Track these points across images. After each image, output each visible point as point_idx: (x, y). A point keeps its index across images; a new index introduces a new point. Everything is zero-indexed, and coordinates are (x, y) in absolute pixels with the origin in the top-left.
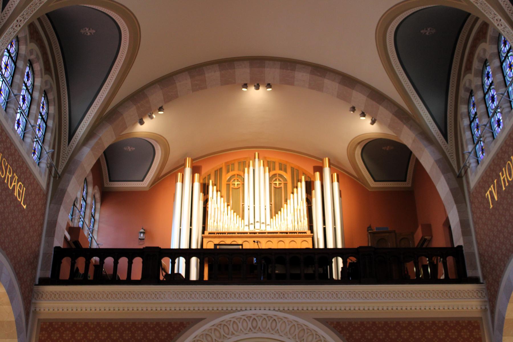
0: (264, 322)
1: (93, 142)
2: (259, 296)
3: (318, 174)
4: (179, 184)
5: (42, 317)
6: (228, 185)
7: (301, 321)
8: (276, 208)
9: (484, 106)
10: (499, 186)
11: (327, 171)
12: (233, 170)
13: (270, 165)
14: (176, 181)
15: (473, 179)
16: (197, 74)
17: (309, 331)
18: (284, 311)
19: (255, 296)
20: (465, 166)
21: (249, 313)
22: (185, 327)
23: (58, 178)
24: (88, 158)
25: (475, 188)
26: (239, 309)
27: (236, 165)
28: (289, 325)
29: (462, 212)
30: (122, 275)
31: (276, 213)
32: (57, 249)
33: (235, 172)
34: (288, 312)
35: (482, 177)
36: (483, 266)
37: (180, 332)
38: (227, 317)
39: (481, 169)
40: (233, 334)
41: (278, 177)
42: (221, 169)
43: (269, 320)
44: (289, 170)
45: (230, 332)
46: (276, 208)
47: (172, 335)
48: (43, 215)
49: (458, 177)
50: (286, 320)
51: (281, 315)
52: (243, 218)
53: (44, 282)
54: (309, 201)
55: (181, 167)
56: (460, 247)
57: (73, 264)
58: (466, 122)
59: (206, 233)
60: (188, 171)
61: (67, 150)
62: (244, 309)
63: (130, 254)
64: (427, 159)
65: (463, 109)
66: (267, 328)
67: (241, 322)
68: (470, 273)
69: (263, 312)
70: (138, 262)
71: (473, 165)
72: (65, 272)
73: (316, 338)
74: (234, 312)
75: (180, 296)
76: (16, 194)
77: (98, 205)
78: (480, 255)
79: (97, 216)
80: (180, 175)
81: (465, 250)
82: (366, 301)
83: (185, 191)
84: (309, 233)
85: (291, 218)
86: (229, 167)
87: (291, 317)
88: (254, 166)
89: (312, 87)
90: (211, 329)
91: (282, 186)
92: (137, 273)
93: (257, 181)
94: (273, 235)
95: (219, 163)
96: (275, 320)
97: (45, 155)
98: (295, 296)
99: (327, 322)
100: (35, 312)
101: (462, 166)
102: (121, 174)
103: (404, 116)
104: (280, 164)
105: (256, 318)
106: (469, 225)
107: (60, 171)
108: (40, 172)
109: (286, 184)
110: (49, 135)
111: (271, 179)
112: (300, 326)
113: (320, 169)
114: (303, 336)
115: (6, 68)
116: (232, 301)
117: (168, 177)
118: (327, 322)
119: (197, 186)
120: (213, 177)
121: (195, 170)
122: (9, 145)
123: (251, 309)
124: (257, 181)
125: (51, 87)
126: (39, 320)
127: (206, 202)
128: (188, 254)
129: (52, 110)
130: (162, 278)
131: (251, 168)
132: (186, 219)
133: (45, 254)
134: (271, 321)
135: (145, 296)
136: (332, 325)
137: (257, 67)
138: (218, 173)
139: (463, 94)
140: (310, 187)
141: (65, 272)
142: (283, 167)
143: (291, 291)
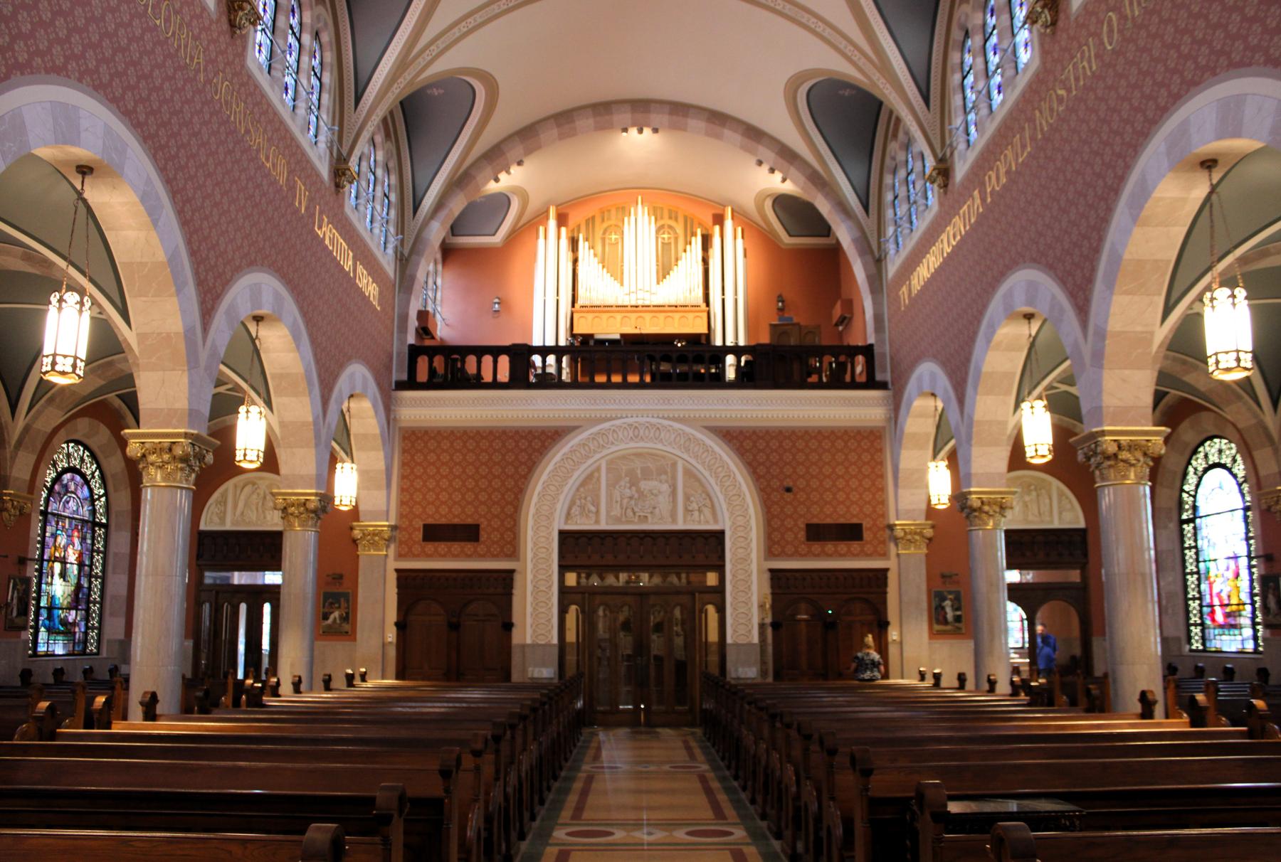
1: (443, 214)
3: (717, 228)
4: (541, 240)
5: (403, 425)
6: (603, 240)
7: (688, 430)
8: (664, 271)
9: (1007, 16)
10: (910, 290)
11: (729, 223)
12: (609, 219)
13: (656, 212)
14: (537, 237)
15: (892, 268)
16: (564, 121)
18: (668, 418)
20: (951, 145)
21: (630, 420)
23: (405, 262)
24: (436, 232)
25: (962, 183)
27: (613, 212)
29: (877, 304)
30: (487, 377)
31: (664, 277)
32: (411, 346)
33: (612, 222)
34: (674, 419)
35: (1023, 94)
36: (892, 372)
38: (607, 425)
39: (972, 156)
41: (666, 229)
42: (593, 218)
44: (681, 219)
46: (664, 271)
48: (393, 309)
49: (877, 262)
51: (666, 423)
52: (622, 285)
53: (401, 386)
54: (705, 261)
55: (542, 217)
56: (871, 346)
57: (431, 362)
58: (957, 77)
59: (577, 306)
60: (552, 223)
61: (413, 225)
63: (496, 351)
64: (844, 234)
65: (955, 57)
68: (879, 377)
70: (504, 361)
71: (962, 146)
72: (422, 376)
76: (327, 242)
77: (440, 267)
78: (892, 359)
79: (439, 282)
80: (541, 229)
81: (877, 350)
83: (549, 247)
84: (703, 306)
85: (683, 284)
86: (604, 213)
87: (677, 425)
88: (636, 214)
89: (708, 134)
91: (672, 241)
92: (504, 375)
93: (640, 233)
94: (659, 308)
95: (590, 210)
97: (324, 128)
100: (395, 419)
101: (948, 142)
102: (475, 247)
103: (818, 180)
104: (670, 211)
106: (883, 321)
107: (406, 252)
108: (320, 158)
109: (676, 239)
110: (325, 97)
111: (657, 232)
113: (719, 220)
115: (265, 10)
117: (528, 228)
119: (564, 242)
120: (583, 228)
121: (562, 220)
122: (198, 11)
124: (640, 233)
125: (326, 24)
126: (400, 428)
127: (575, 261)
128: (558, 351)
129: (329, 57)
130: (532, 379)
131: (633, 218)
132: (553, 293)
133: (398, 354)
137: (642, 110)
138: (590, 221)
139: (957, 35)
140: (706, 242)
141: (422, 376)
142: (673, 216)
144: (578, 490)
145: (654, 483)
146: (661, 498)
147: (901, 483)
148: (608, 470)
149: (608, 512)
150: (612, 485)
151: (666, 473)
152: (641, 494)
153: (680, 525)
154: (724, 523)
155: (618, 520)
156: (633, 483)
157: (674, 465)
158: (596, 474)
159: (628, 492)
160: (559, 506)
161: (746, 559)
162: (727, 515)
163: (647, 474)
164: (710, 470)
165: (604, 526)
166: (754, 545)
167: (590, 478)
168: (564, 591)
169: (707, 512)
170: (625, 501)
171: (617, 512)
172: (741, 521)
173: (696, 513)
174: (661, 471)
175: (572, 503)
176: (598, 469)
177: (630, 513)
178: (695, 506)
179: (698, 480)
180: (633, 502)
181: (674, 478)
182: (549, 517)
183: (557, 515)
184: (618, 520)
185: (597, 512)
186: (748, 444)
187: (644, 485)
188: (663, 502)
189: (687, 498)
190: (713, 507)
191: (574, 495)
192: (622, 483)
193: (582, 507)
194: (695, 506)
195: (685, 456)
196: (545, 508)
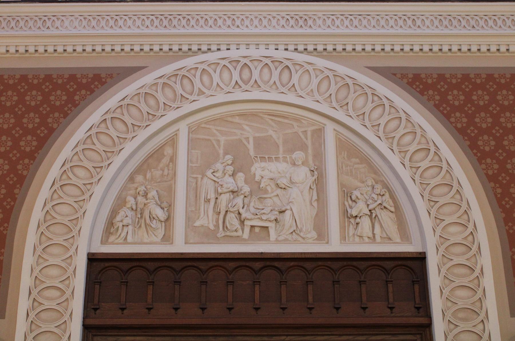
0: (266, 70)
2: (256, 22)
7: (342, 69)
17: (357, 87)
19: (247, 22)
21: (234, 54)
22: (103, 83)
26: (195, 48)
28: (317, 76)
37: (92, 91)
38: (190, 62)
40: (201, 93)
43: (276, 69)
45: (196, 90)
47: (77, 98)
50: (310, 68)
62: (204, 48)
66: (272, 82)
67: (218, 71)
69: (262, 51)
73: (373, 101)
74: (195, 53)
75: (94, 23)
82: (473, 32)
87: (321, 63)
90: (156, 84)
96: (287, 67)
98: (329, 22)
99: (395, 75)
105: (249, 64)
112: (338, 79)
114: (346, 97)
116: (200, 31)
118: (395, 75)
123: (219, 50)
134: (279, 69)
135: (22, 23)
136: (405, 81)
143: (320, 14)
144: (131, 179)
145: (282, 166)
146: (294, 192)
147: (262, 228)
148: (192, 143)
149: (189, 220)
150: (196, 172)
151: (303, 148)
152: (257, 190)
153: (335, 245)
154: (424, 238)
155: (210, 235)
156: (240, 165)
157: (319, 133)
158: (168, 151)
159: (229, 183)
160: (91, 207)
161: (475, 311)
162: (427, 223)
163: (266, 150)
164: (390, 139)
165: (179, 246)
166: (488, 282)
167: (158, 159)
168: (419, 92)
169: (386, 218)
170: (224, 199)
171: (206, 220)
172: (456, 235)
173: (366, 222)
174: (295, 144)
175: (120, 203)
176: (173, 141)
177: (233, 220)
178: (360, 208)
179: (365, 160)
180: (239, 201)
181: (319, 156)
182: (71, 228)
183: (86, 224)
184: (210, 235)
185: (168, 220)
186: (456, 98)
187: (263, 170)
188: (300, 203)
189: (347, 194)
190: (398, 211)
191: (124, 188)
192: (219, 166)
193: (139, 212)
194: (360, 208)
195: (340, 115)
196: (64, 209)
